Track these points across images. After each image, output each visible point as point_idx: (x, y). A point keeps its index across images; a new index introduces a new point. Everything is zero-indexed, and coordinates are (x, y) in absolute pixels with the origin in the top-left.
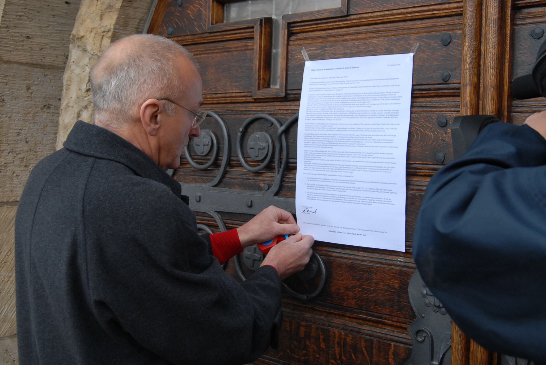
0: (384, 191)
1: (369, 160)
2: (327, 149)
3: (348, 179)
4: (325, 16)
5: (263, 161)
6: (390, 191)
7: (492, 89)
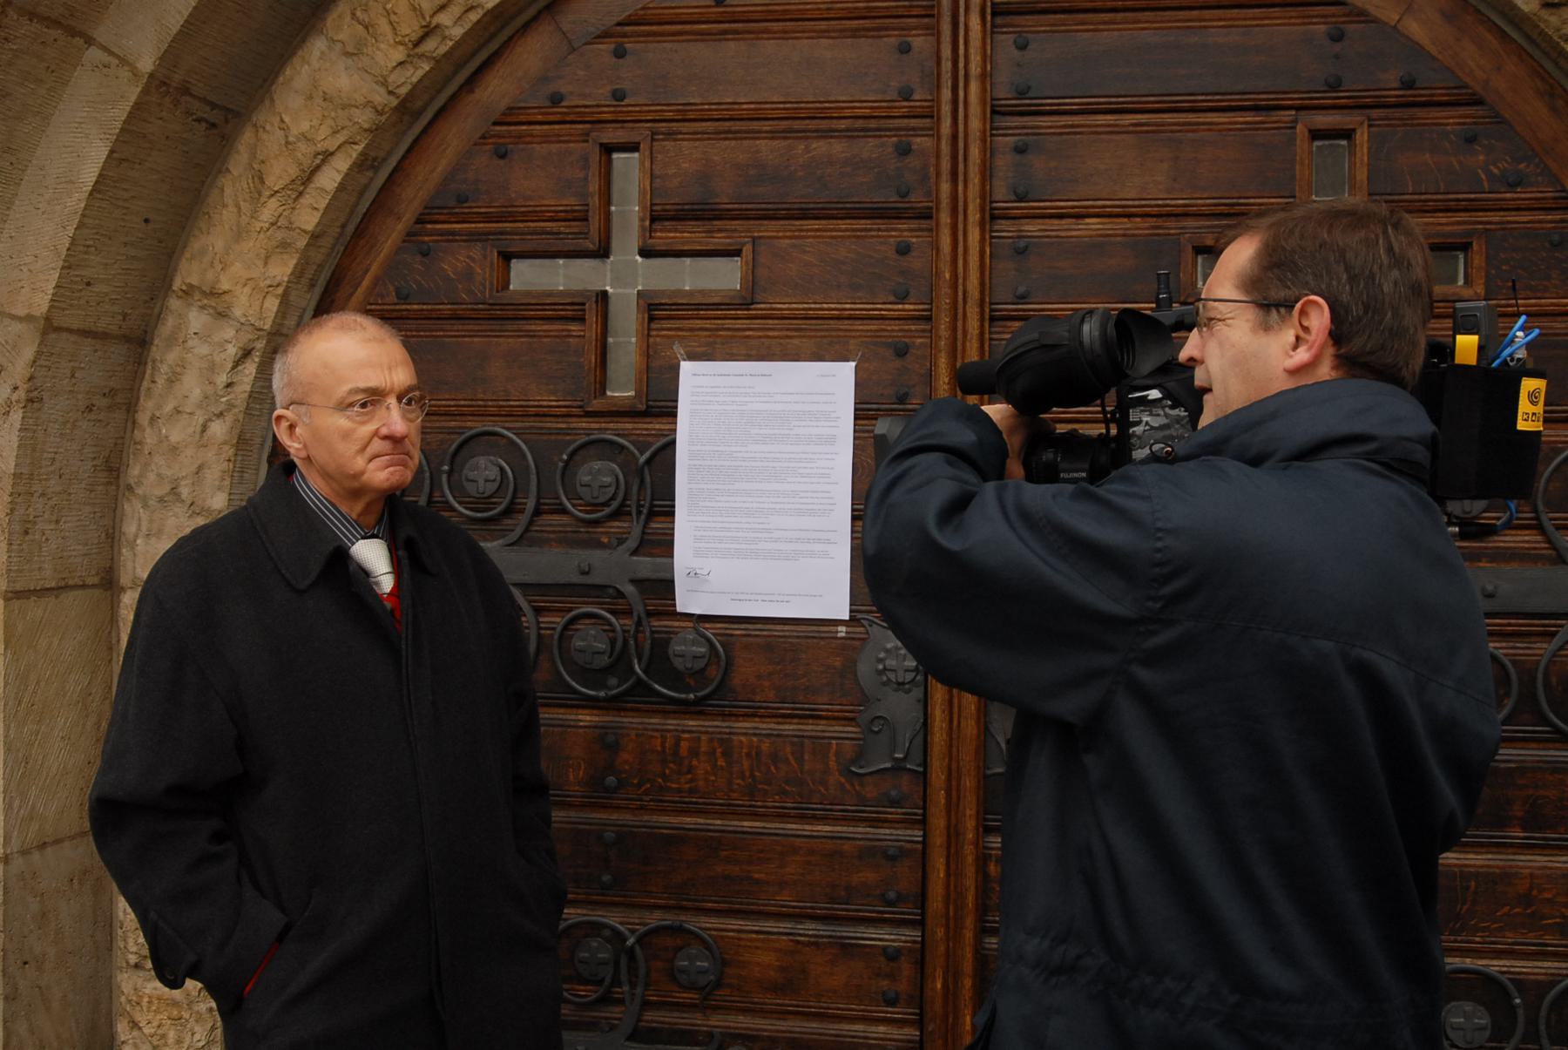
4: (716, 300)
6: (828, 541)
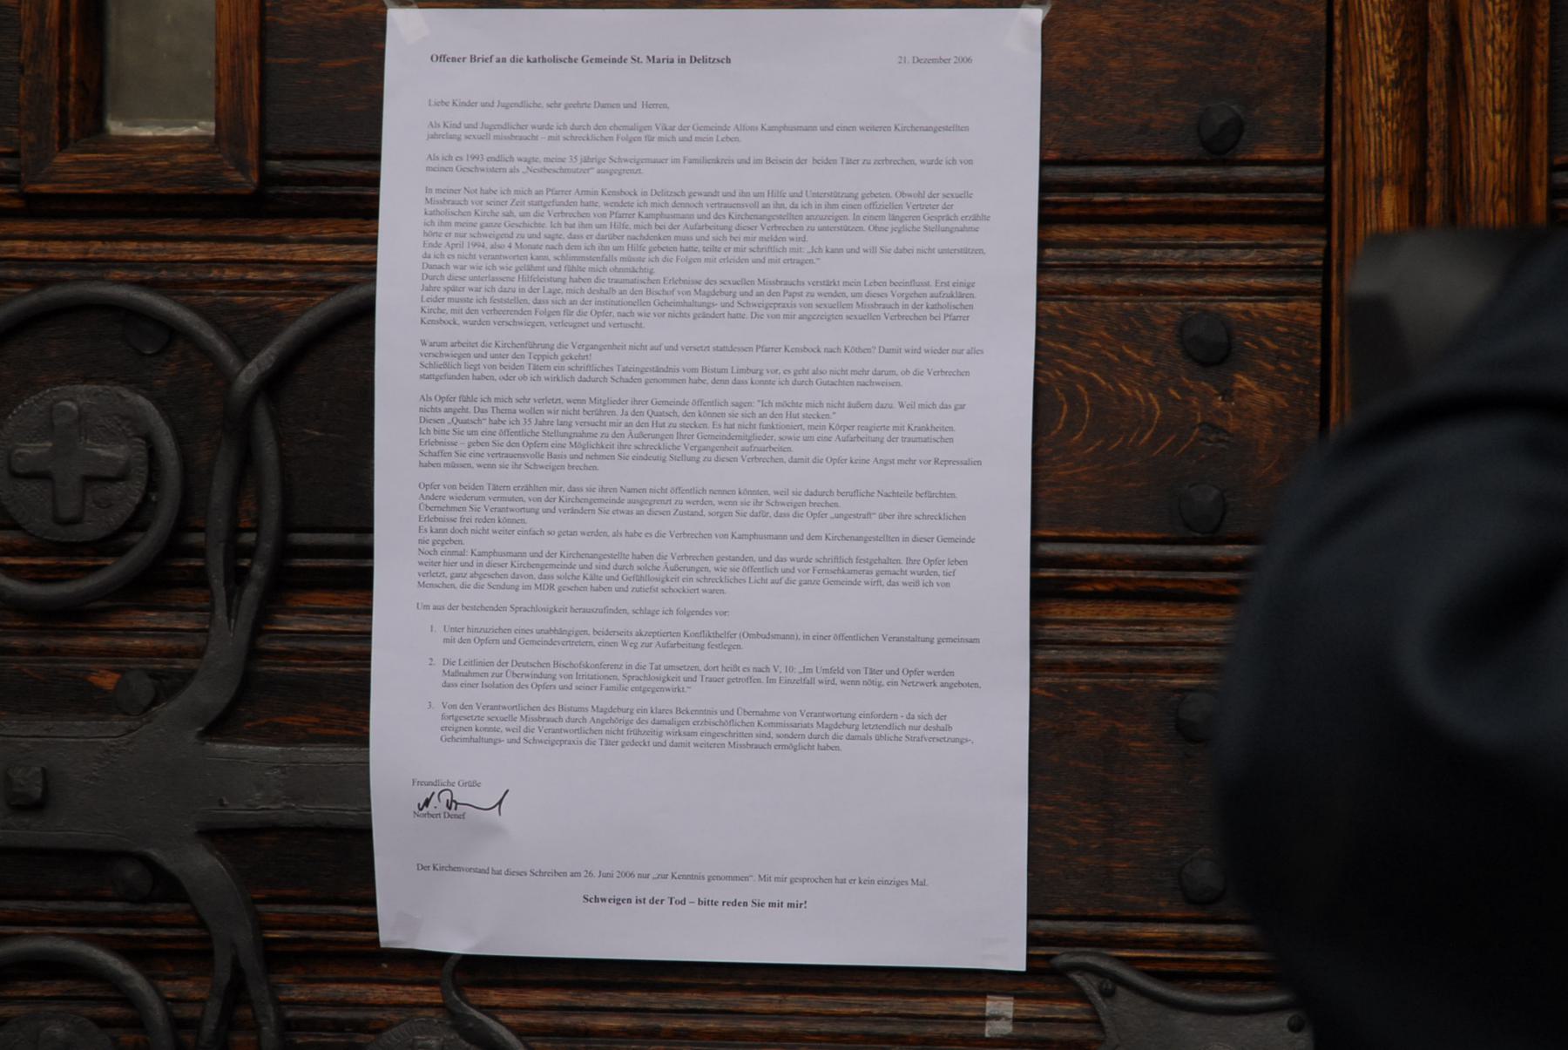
0: (911, 676)
1: (819, 527)
2: (565, 478)
3: (696, 624)
5: (111, 544)
6: (945, 679)
7: (1503, 204)
